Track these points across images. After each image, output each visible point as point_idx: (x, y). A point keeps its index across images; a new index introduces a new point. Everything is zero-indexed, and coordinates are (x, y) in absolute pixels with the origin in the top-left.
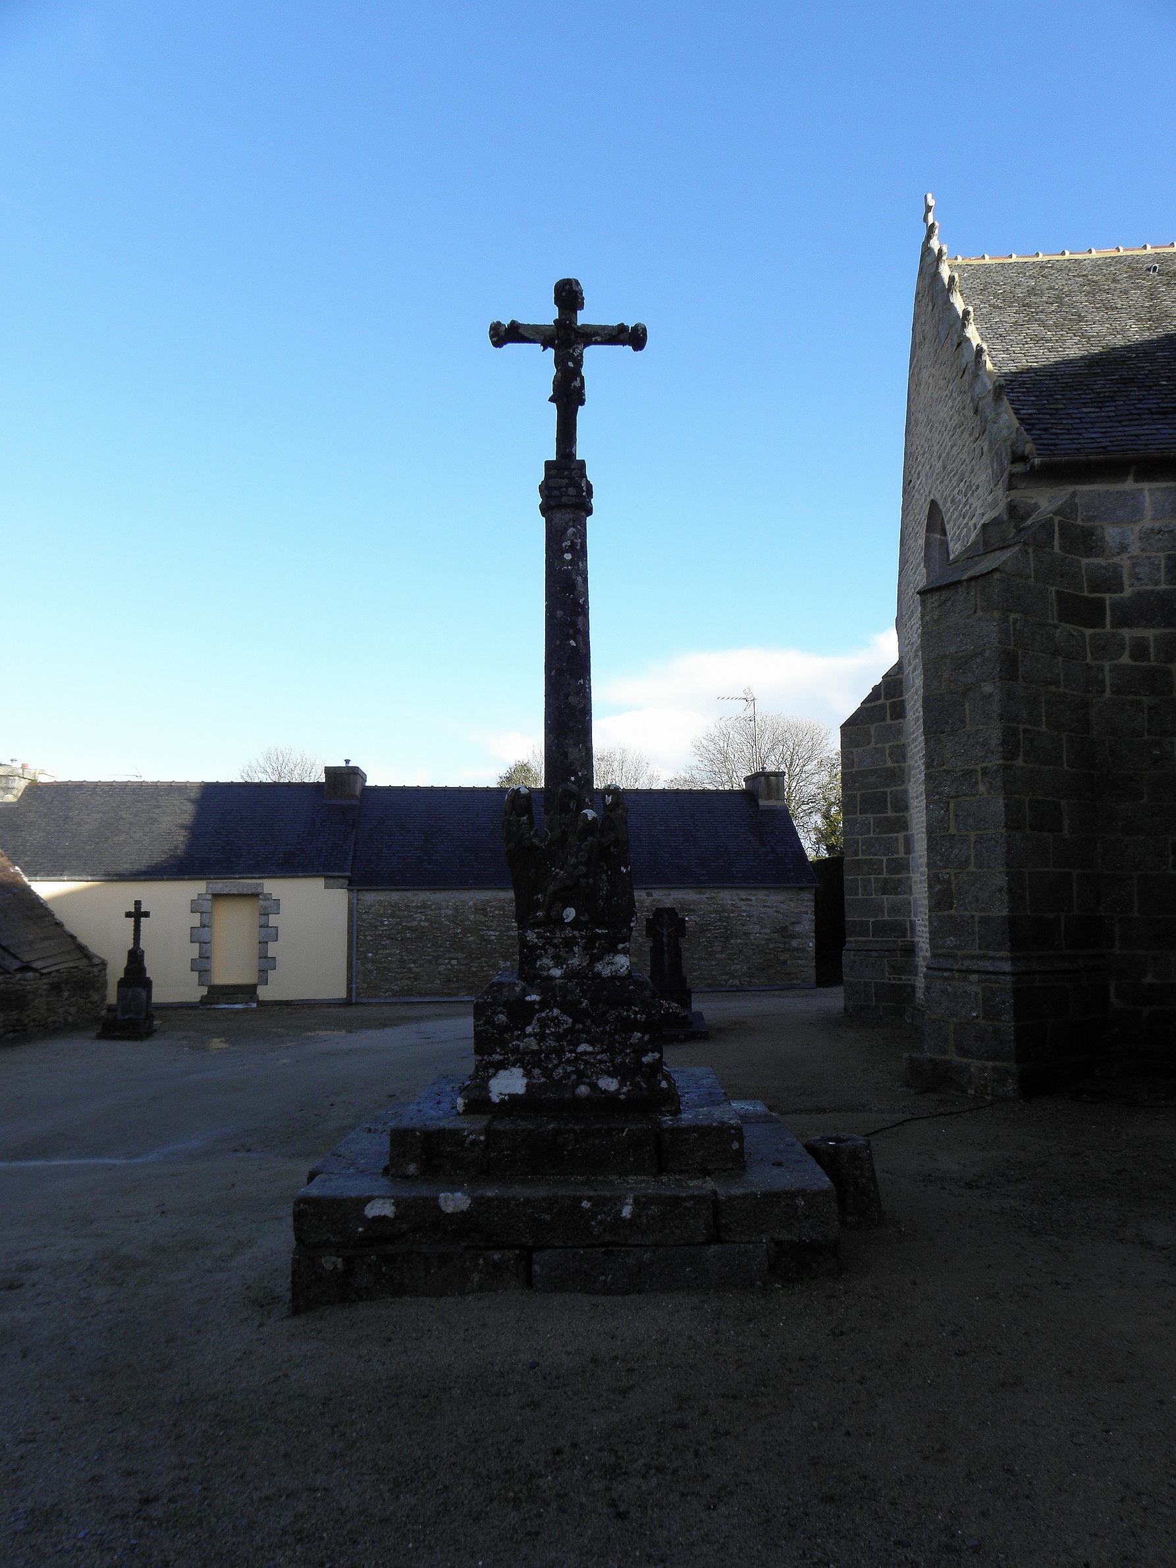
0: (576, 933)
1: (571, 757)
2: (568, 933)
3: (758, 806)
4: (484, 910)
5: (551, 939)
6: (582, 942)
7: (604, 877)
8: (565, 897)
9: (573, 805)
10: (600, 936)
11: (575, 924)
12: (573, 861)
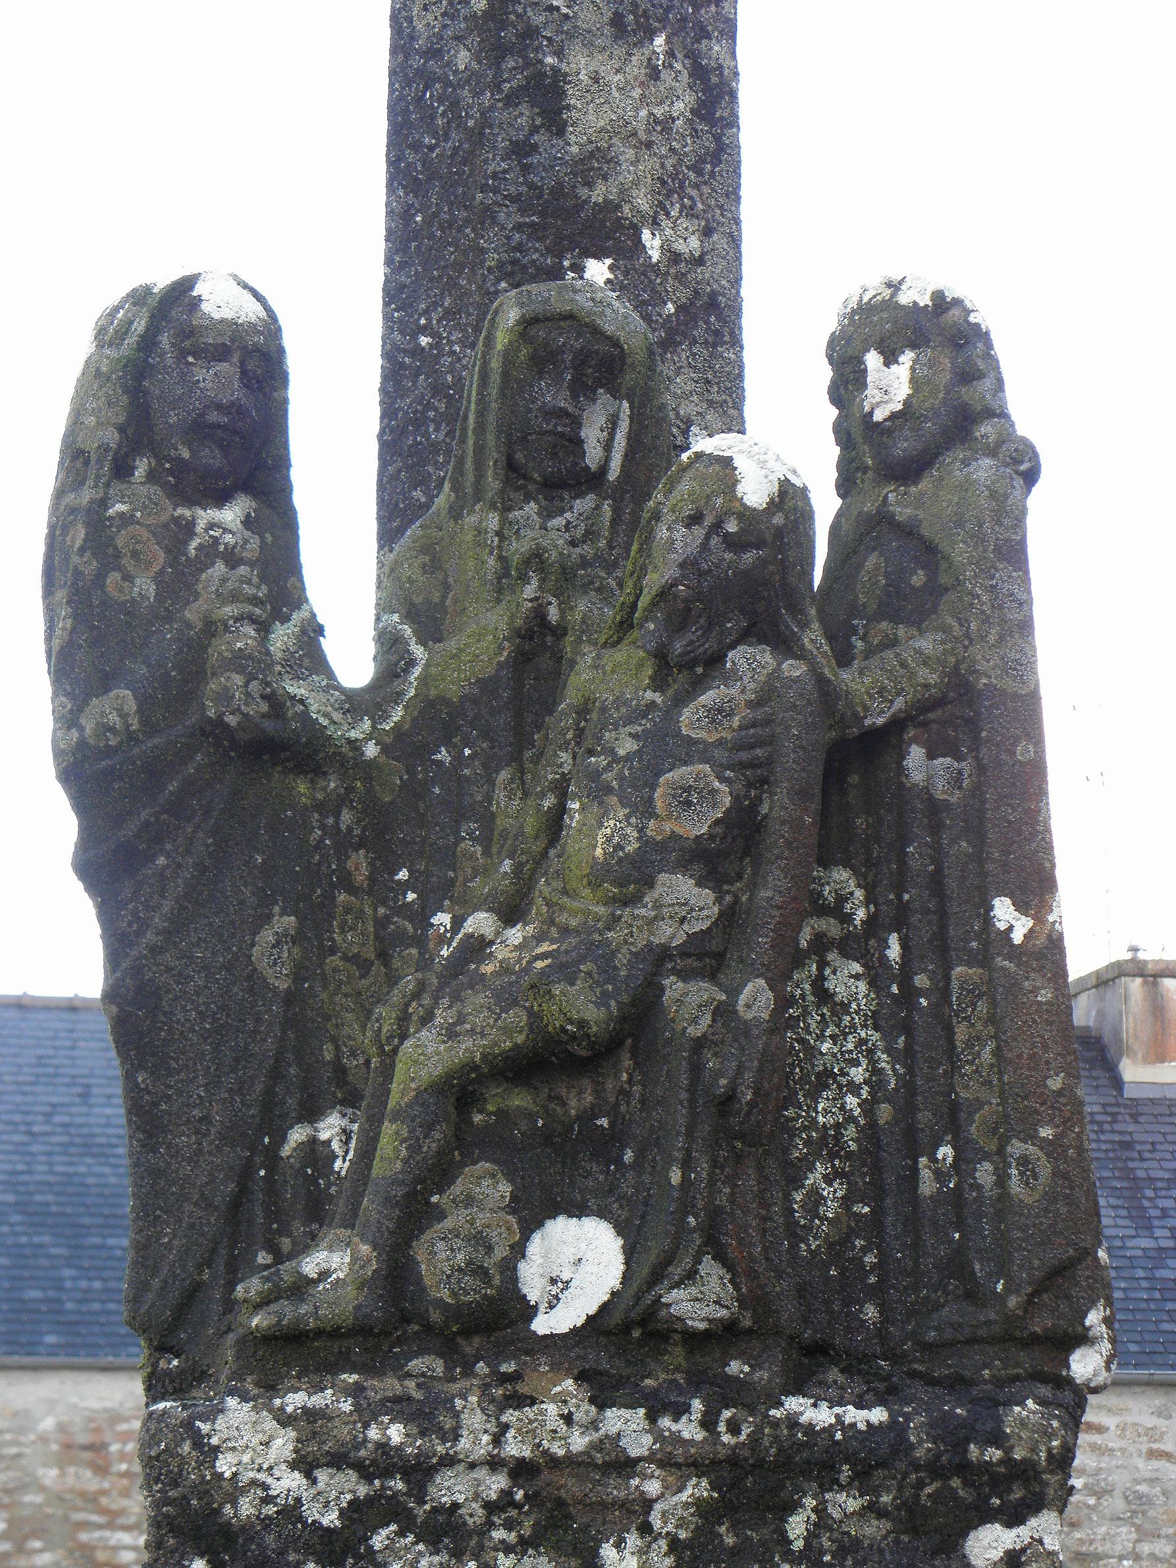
0: (627, 1425)
1: (588, 119)
2: (561, 1420)
3: (1117, 1083)
4: (97, 1448)
5: (420, 1472)
6: (675, 1503)
7: (847, 980)
8: (550, 1107)
9: (603, 435)
10: (820, 1460)
11: (624, 1347)
12: (601, 833)
